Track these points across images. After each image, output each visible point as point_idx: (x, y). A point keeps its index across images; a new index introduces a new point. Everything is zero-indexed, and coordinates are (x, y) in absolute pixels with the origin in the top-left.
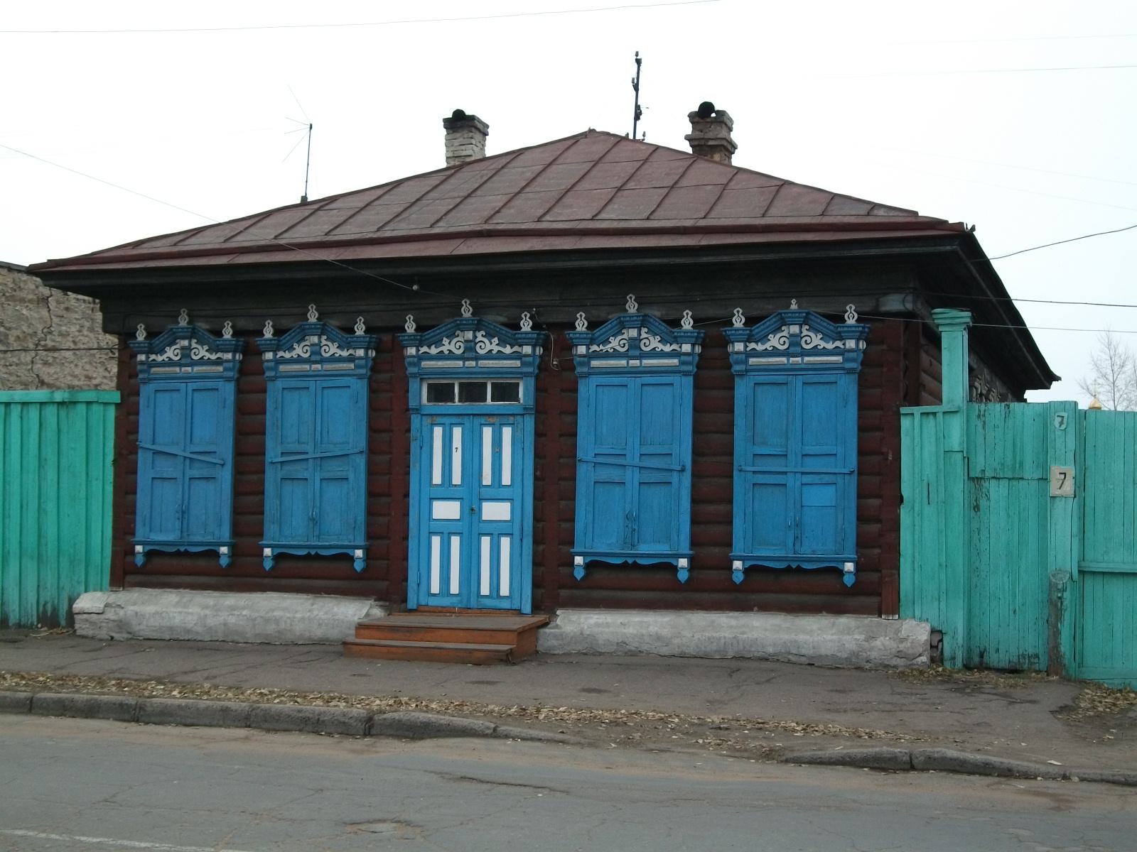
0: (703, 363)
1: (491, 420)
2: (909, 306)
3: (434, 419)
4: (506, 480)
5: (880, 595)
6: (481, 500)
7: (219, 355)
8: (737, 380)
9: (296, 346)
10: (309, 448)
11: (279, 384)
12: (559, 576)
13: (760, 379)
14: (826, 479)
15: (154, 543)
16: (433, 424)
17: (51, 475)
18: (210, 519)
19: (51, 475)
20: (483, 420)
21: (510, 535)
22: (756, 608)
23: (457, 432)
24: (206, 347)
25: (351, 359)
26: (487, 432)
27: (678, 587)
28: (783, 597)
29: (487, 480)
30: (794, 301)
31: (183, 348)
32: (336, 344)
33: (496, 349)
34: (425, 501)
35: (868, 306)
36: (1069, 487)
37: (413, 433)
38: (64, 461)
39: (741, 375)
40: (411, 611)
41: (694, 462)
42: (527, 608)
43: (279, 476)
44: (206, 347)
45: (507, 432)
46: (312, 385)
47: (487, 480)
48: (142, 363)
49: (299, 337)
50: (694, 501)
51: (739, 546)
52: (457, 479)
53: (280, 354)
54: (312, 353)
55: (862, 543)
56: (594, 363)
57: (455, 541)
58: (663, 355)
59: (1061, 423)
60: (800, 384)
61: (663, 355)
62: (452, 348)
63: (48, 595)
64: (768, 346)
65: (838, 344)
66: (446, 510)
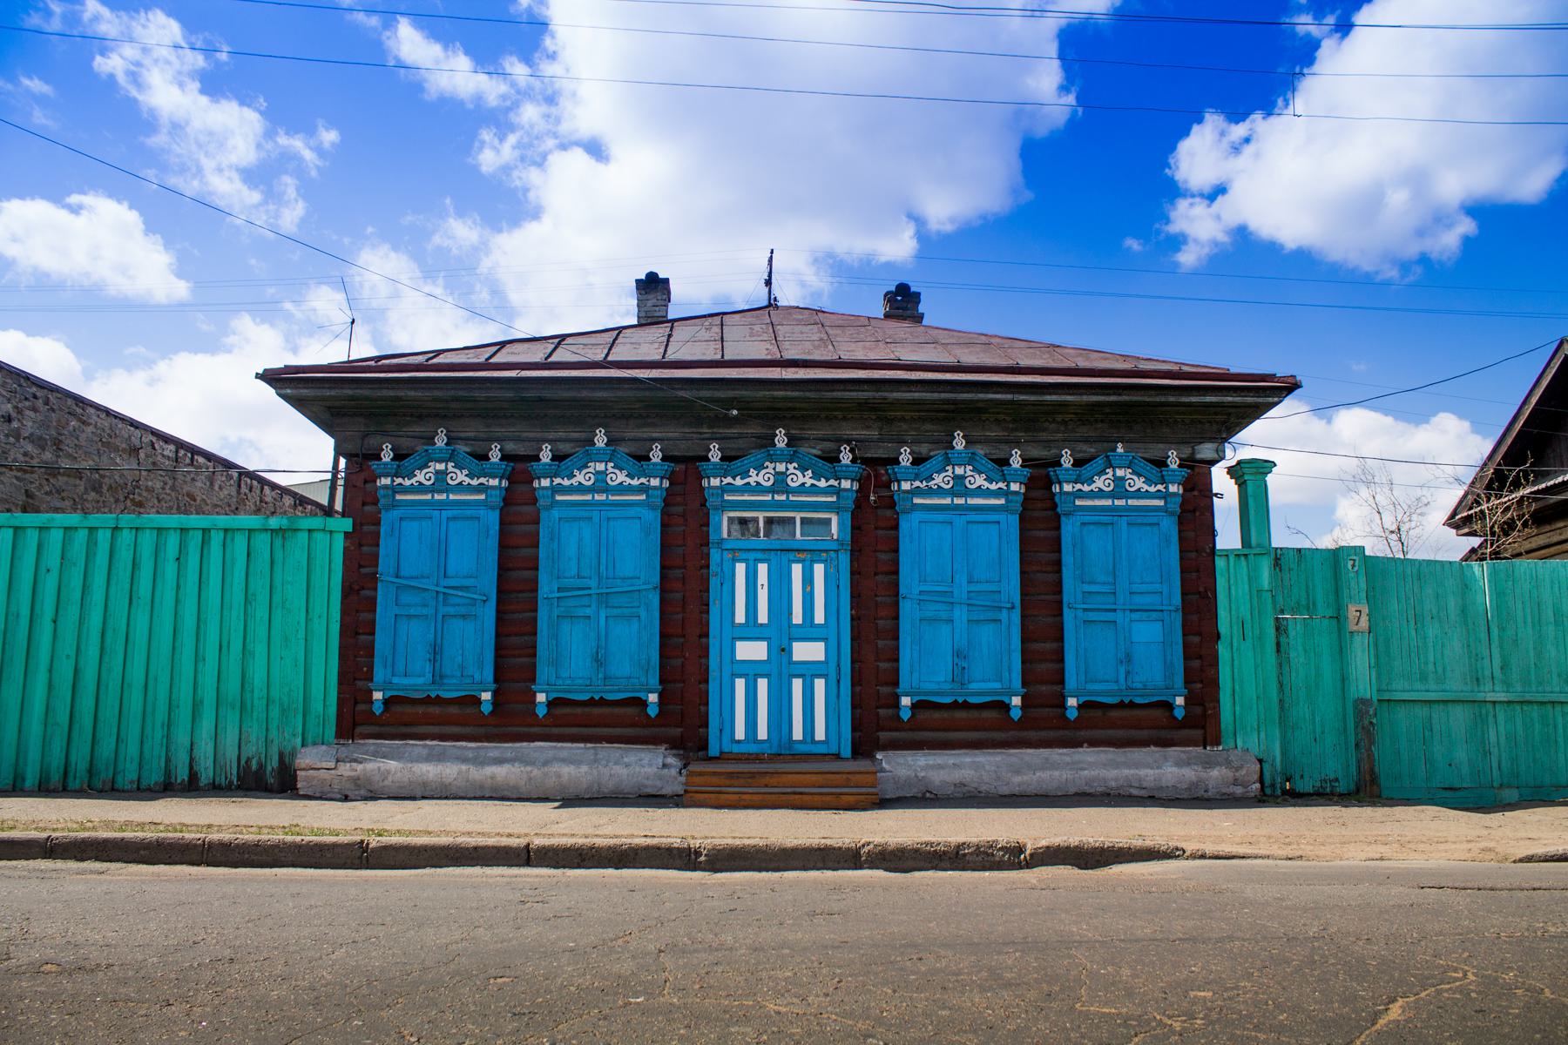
0: (669, 499)
1: (801, 556)
3: (736, 555)
4: (819, 618)
5: (1203, 727)
6: (792, 639)
7: (483, 480)
8: (1063, 519)
9: (576, 472)
10: (593, 583)
11: (556, 513)
12: (882, 717)
13: (1087, 519)
14: (1154, 615)
15: (919, 694)
16: (735, 560)
17: (261, 612)
18: (469, 658)
19: (261, 612)
20: (791, 556)
21: (825, 676)
23: (763, 569)
24: (465, 472)
25: (643, 489)
26: (797, 569)
27: (481, 720)
28: (1111, 732)
29: (797, 618)
30: (1120, 445)
31: (437, 472)
32: (625, 472)
33: (809, 482)
34: (726, 643)
35: (1186, 452)
36: (1364, 623)
37: (713, 567)
38: (277, 598)
39: (1068, 514)
41: (1022, 601)
42: (847, 751)
43: (556, 612)
44: (465, 472)
45: (819, 569)
46: (596, 515)
47: (797, 618)
48: (386, 487)
49: (581, 463)
50: (1025, 639)
51: (1071, 681)
52: (763, 618)
53: (557, 481)
55: (1188, 680)
56: (917, 501)
57: (763, 684)
58: (1148, 495)
60: (1124, 526)
61: (1148, 495)
62: (760, 479)
63: (250, 750)
65: (1160, 487)
66: (752, 651)
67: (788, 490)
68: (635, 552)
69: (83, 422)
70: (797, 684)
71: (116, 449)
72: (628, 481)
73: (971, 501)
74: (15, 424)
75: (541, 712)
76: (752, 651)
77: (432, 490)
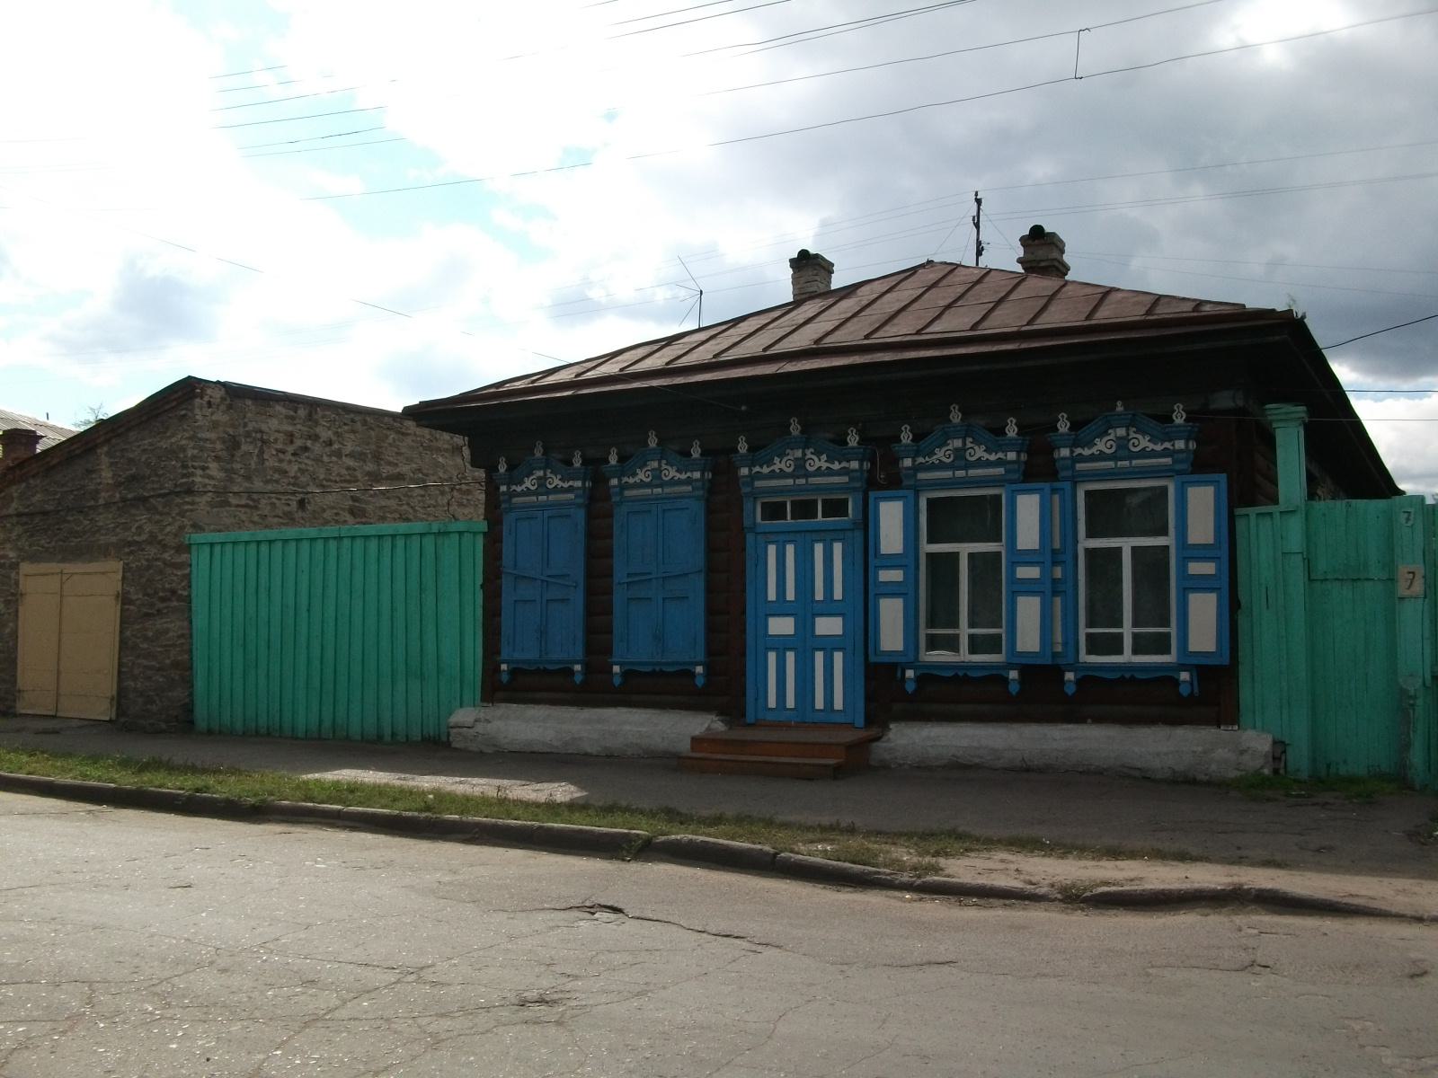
2: (1240, 403)
3: (770, 537)
7: (571, 483)
17: (430, 599)
22: (1089, 721)
23: (790, 549)
40: (749, 725)
54: (1119, 447)
56: (921, 476)
57: (790, 656)
58: (1153, 454)
59: (1408, 519)
61: (1153, 454)
62: (782, 466)
64: (1094, 450)
67: (807, 475)
68: (685, 543)
69: (403, 434)
70: (819, 656)
71: (439, 450)
72: (678, 475)
73: (972, 472)
74: (336, 446)
75: (617, 681)
76: (781, 626)
77: (535, 493)
